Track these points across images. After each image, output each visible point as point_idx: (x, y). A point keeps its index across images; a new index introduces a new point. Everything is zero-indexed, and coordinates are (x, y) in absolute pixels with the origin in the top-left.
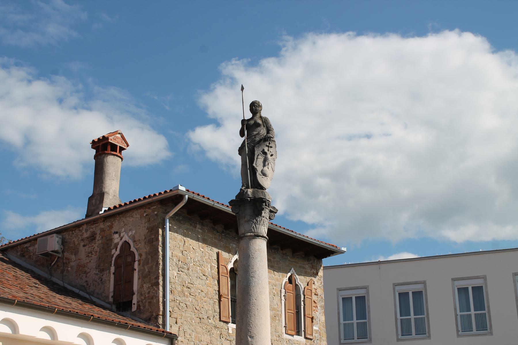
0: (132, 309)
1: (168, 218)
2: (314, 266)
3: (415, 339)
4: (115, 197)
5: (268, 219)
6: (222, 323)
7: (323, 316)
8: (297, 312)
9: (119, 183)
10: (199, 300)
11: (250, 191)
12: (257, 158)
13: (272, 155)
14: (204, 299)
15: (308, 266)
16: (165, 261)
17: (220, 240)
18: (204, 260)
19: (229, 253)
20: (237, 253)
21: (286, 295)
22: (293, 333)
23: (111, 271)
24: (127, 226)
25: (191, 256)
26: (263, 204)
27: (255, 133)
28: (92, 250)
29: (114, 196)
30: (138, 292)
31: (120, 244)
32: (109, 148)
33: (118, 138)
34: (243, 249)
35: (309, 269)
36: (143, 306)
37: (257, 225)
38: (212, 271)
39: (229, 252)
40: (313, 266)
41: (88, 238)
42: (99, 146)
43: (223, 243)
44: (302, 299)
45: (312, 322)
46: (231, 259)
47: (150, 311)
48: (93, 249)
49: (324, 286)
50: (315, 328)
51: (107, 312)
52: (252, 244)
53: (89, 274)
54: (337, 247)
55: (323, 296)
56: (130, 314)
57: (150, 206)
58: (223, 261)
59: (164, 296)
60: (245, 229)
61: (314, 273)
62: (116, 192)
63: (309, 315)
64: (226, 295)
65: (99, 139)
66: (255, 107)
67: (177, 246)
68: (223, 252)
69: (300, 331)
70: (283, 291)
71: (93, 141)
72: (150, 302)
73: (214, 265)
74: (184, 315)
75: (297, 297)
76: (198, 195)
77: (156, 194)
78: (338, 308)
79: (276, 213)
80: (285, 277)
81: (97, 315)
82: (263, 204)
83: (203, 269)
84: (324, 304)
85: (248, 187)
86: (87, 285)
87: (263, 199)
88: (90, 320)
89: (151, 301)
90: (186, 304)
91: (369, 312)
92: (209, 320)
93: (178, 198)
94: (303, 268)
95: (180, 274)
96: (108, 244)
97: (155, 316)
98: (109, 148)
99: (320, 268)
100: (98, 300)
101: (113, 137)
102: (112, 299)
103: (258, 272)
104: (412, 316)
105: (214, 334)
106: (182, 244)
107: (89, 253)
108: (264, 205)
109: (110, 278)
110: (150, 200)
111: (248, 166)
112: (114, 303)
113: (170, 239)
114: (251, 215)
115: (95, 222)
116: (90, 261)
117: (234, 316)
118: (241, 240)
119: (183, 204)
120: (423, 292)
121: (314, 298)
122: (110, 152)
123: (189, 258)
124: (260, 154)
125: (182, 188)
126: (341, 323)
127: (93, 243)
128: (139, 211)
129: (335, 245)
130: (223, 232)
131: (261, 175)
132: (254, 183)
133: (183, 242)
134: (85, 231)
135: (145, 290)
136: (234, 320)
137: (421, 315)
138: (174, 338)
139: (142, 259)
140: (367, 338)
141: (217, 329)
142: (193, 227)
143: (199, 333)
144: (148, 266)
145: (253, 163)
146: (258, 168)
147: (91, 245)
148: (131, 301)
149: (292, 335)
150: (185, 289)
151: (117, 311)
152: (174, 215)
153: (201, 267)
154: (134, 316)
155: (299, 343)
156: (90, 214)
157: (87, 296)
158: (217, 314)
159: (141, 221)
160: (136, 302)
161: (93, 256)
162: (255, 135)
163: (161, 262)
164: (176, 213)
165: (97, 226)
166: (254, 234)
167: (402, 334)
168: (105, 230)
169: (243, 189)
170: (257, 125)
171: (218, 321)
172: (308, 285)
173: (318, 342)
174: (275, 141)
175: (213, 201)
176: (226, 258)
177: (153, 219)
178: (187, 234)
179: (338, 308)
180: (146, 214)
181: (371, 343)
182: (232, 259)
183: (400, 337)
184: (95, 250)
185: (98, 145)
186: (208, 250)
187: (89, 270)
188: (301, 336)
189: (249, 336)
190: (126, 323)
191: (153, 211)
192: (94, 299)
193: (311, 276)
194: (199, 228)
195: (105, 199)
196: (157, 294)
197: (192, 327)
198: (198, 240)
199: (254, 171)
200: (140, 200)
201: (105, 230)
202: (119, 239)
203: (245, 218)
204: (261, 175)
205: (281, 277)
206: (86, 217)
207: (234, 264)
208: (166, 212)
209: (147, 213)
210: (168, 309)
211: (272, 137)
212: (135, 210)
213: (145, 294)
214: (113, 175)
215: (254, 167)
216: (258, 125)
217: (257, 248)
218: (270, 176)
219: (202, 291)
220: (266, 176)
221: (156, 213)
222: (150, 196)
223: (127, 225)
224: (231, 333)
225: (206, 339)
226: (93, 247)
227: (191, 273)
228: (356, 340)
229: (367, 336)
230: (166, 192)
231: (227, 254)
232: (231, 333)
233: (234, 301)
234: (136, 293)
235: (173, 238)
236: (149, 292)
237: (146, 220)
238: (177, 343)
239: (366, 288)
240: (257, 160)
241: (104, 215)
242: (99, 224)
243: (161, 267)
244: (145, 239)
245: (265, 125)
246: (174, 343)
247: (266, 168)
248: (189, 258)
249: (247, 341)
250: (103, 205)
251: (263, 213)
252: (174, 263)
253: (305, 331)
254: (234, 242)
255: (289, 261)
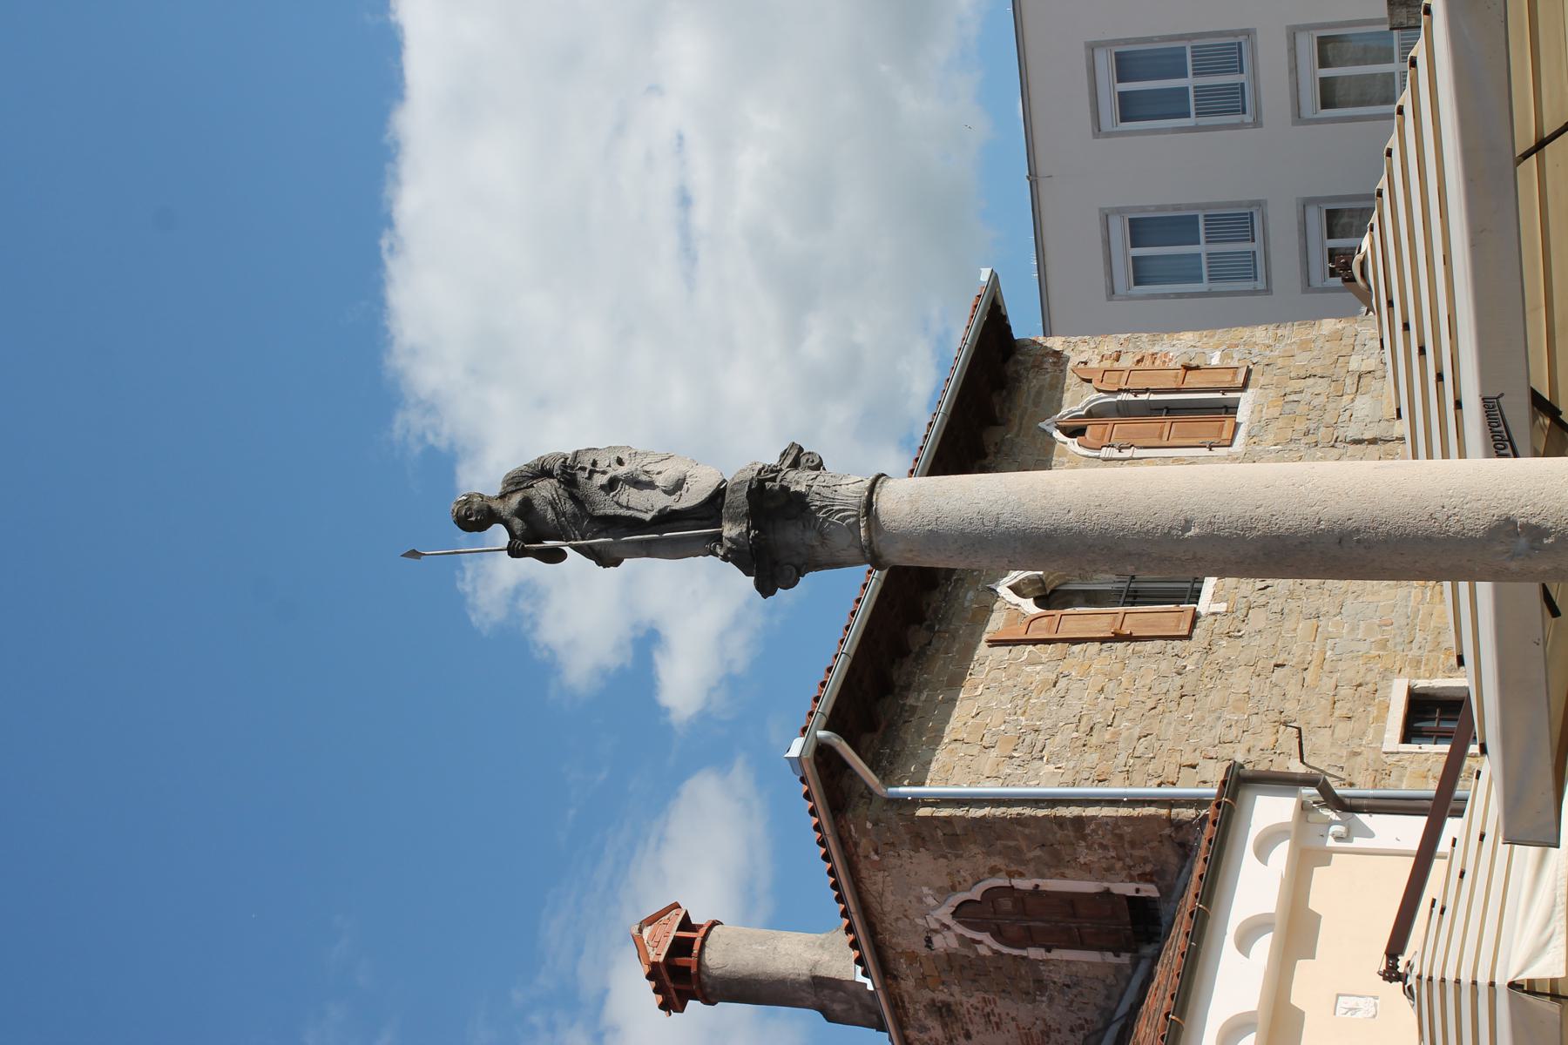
0: (1154, 898)
1: (884, 790)
2: (1034, 361)
3: (1255, 76)
4: (826, 946)
5: (818, 472)
6: (1197, 632)
7: (1181, 337)
8: (1167, 413)
9: (784, 933)
10: (1129, 699)
11: (730, 530)
12: (628, 508)
13: (620, 462)
14: (1125, 685)
15: (1035, 381)
16: (1010, 800)
17: (954, 637)
18: (1010, 683)
19: (992, 611)
20: (993, 586)
21: (1117, 446)
22: (1228, 424)
23: (1040, 959)
24: (911, 911)
25: (997, 723)
26: (767, 488)
27: (550, 515)
28: (979, 1012)
29: (821, 946)
30: (1103, 879)
31: (960, 930)
32: (682, 961)
33: (652, 936)
34: (911, 551)
35: (1043, 377)
36: (1144, 864)
37: (836, 508)
38: (1044, 660)
39: (988, 610)
40: (1033, 367)
41: (945, 1026)
42: (675, 989)
43: (961, 627)
44: (1131, 397)
45: (1197, 368)
46: (1008, 606)
47: (1157, 843)
48: (977, 1008)
49: (1093, 334)
50: (1215, 361)
51: (1159, 972)
52: (893, 524)
53: (1051, 1023)
54: (979, 296)
55: (1123, 336)
56: (1166, 905)
57: (851, 843)
58: (1014, 627)
59: (1114, 802)
60: (849, 547)
61: (1054, 362)
62: (812, 942)
63: (1176, 377)
64: (1114, 620)
65: (656, 991)
66: (471, 516)
67: (968, 762)
68: (988, 629)
69: (1226, 404)
70: (1105, 452)
71: (663, 1006)
72: (1133, 845)
73: (1026, 653)
74: (1171, 743)
75: (1124, 411)
76: (817, 699)
77: (813, 825)
78: (1165, 296)
79: (801, 449)
80: (1064, 448)
81: (1167, 1004)
82: (767, 488)
83: (1037, 687)
84: (1146, 335)
85: (718, 538)
86: (1081, 1027)
87: (753, 487)
88: (1181, 1022)
89: (1128, 842)
90: (1140, 738)
91: (1176, 207)
92: (1187, 669)
93: (824, 758)
94: (1039, 393)
95: (1052, 754)
96: (962, 967)
97: (1173, 829)
98: (682, 961)
99: (1041, 345)
100: (1125, 997)
101: (650, 949)
102: (1122, 954)
103: (982, 505)
104: (1189, 82)
105: (1228, 655)
106: (962, 750)
107: (990, 1021)
108: (771, 484)
109: (1062, 960)
110: (831, 842)
111: (642, 537)
112: (1136, 951)
113: (946, 782)
114: (804, 526)
115: (897, 1004)
116: (1013, 1019)
117: (1176, 597)
118: (881, 557)
119: (844, 743)
120: (1117, 50)
121: (1127, 362)
122: (694, 959)
123: (1003, 728)
124: (615, 499)
125: (796, 747)
126: (1206, 290)
127: (958, 1011)
128: (864, 873)
129: (974, 300)
130: (931, 628)
131: (681, 495)
132: (708, 519)
133: (958, 745)
134: (926, 1032)
135: (1096, 860)
136: (1188, 597)
137: (1185, 56)
138: (1238, 774)
139: (1003, 867)
140: (1252, 213)
141: (1214, 648)
142: (912, 715)
143: (1224, 699)
144: (1025, 848)
145: (641, 521)
146: (659, 506)
147: (967, 1016)
148: (1130, 899)
149: (1237, 426)
150: (1094, 740)
151: (1158, 942)
152: (877, 772)
153: (1032, 692)
154: (1172, 892)
155: (1257, 408)
156: (875, 1018)
157: (1114, 1029)
158: (1169, 647)
159: (894, 868)
160: (1131, 884)
161: (996, 1011)
162: (557, 514)
163: (1014, 811)
164: (870, 767)
165: (910, 997)
166: (863, 517)
167: (1239, 111)
168: (922, 974)
169: (722, 554)
170: (526, 509)
171: (1192, 642)
172: (1089, 381)
173: (1255, 351)
174: (577, 452)
175: (836, 656)
176: (1007, 620)
177: (888, 835)
178: (933, 734)
179: (1165, 296)
180: (872, 853)
181: (1265, 202)
182: (1010, 603)
183: (1248, 118)
184: (978, 1005)
185: (674, 994)
186: (981, 672)
187: (1038, 1022)
188: (1238, 399)
189: (1182, 535)
190: (1191, 914)
191: (865, 832)
192: (1124, 1008)
193: (1063, 371)
194: (918, 699)
195: (832, 975)
196: (1107, 824)
197: (1207, 720)
198: (951, 702)
199: (667, 519)
200: (831, 872)
201: (922, 974)
202: (946, 933)
203: (813, 547)
204: (681, 495)
205: (1065, 460)
206: (884, 1031)
207: (1024, 596)
208: (869, 796)
209: (871, 849)
210: (1152, 790)
211: (565, 462)
212: (861, 885)
213: (1107, 859)
214: (761, 951)
215: (654, 518)
216: (527, 504)
217: (906, 508)
218: (683, 468)
219: (1102, 689)
220: (685, 479)
221: (869, 825)
222: (822, 843)
223: (906, 910)
224: (1225, 605)
225: (1244, 680)
226: (972, 1011)
227: (1049, 723)
228: (1256, 246)
229: (1246, 214)
230: (807, 796)
231: (994, 615)
232: (1225, 605)
233: (1134, 597)
234: (1106, 885)
235: (943, 776)
236: (1103, 847)
237: (891, 853)
238: (1252, 764)
239: (1107, 216)
240: (633, 509)
241: (878, 976)
242: (903, 994)
243: (1028, 811)
244: (945, 857)
245: (525, 485)
246: (1251, 774)
247: (660, 481)
248: (1003, 728)
249: (1200, 539)
250: (848, 978)
251: (798, 488)
252: (1018, 772)
253: (1225, 390)
254: (961, 595)
255: (1018, 436)
